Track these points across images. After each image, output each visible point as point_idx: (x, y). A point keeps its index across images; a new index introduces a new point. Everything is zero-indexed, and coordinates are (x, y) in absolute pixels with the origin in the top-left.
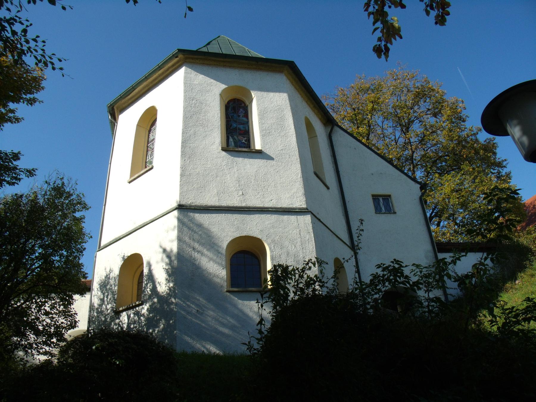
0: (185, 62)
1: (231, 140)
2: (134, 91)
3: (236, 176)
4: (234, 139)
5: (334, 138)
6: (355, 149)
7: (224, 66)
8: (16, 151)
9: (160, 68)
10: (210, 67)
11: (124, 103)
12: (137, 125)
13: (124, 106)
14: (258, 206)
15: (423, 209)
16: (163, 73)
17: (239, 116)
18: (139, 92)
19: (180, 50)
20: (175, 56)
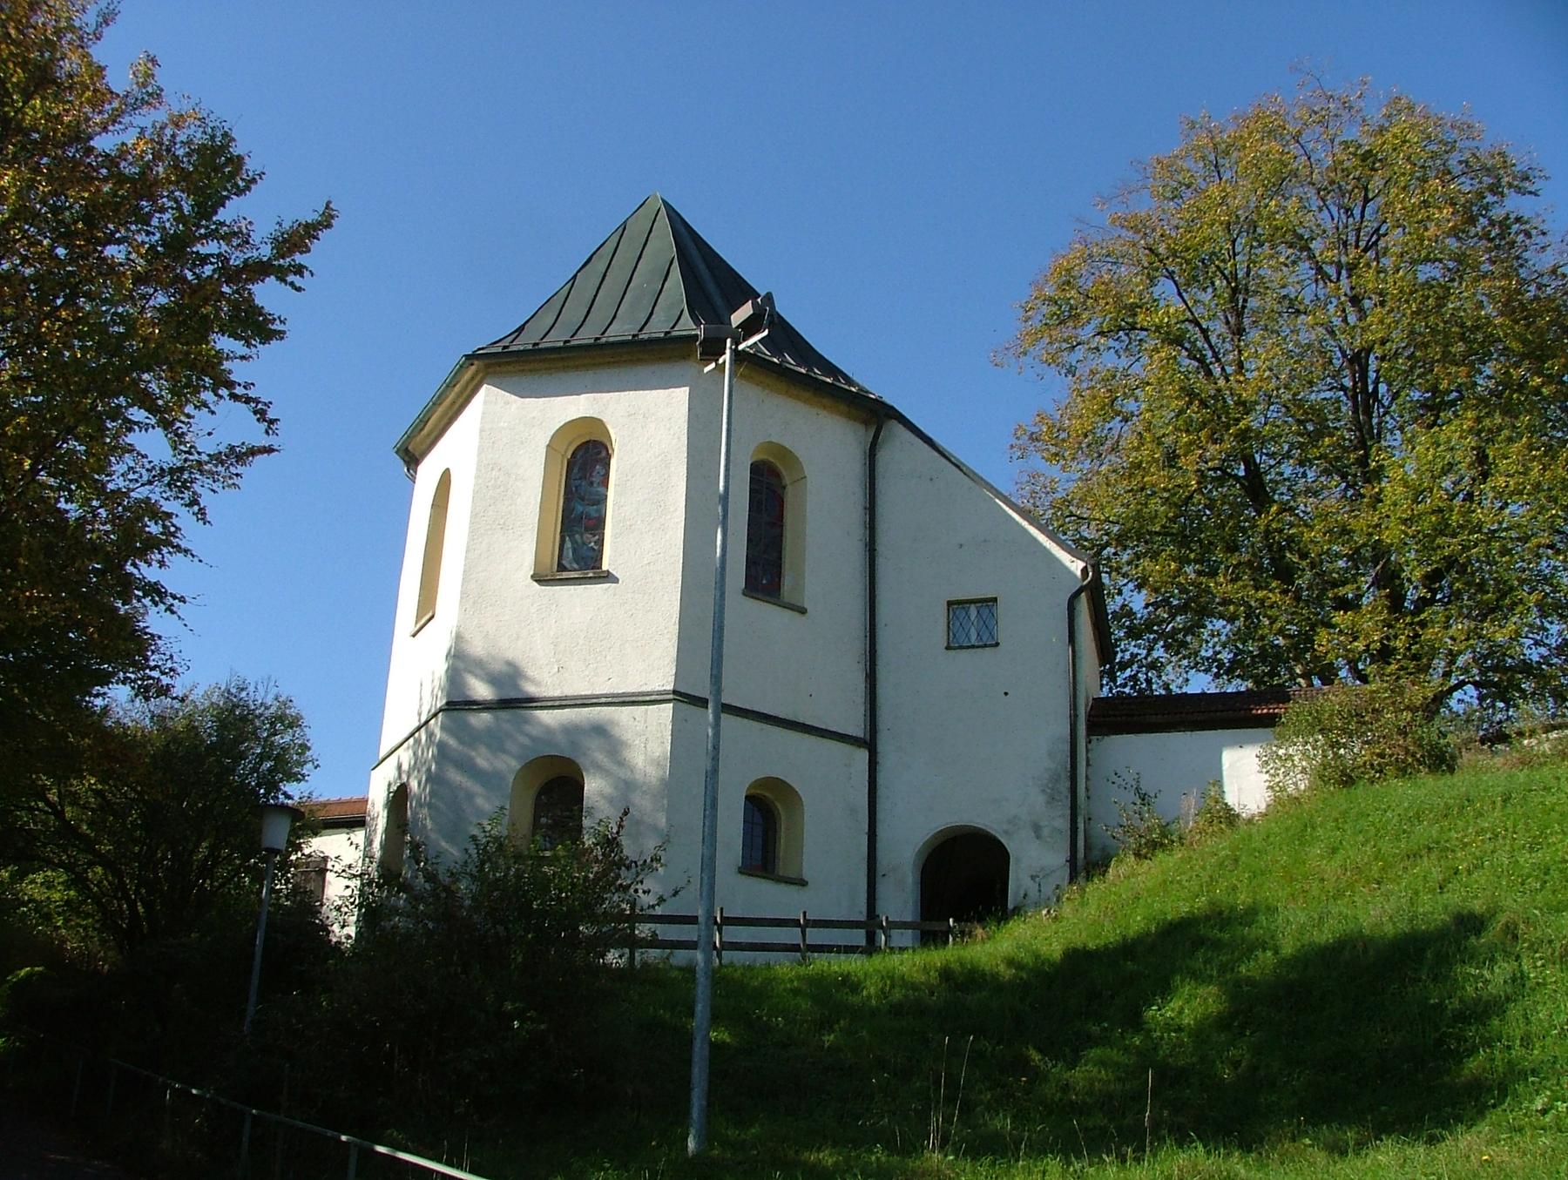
0: (488, 374)
1: (568, 545)
2: (425, 425)
3: (552, 634)
4: (574, 542)
5: (883, 457)
6: (931, 480)
7: (565, 369)
8: (103, 64)
9: (450, 385)
10: (536, 377)
11: (421, 443)
12: (548, 446)
13: (424, 447)
14: (583, 693)
15: (875, 633)
16: (461, 392)
17: (592, 483)
18: (436, 425)
19: (468, 357)
20: (462, 368)
